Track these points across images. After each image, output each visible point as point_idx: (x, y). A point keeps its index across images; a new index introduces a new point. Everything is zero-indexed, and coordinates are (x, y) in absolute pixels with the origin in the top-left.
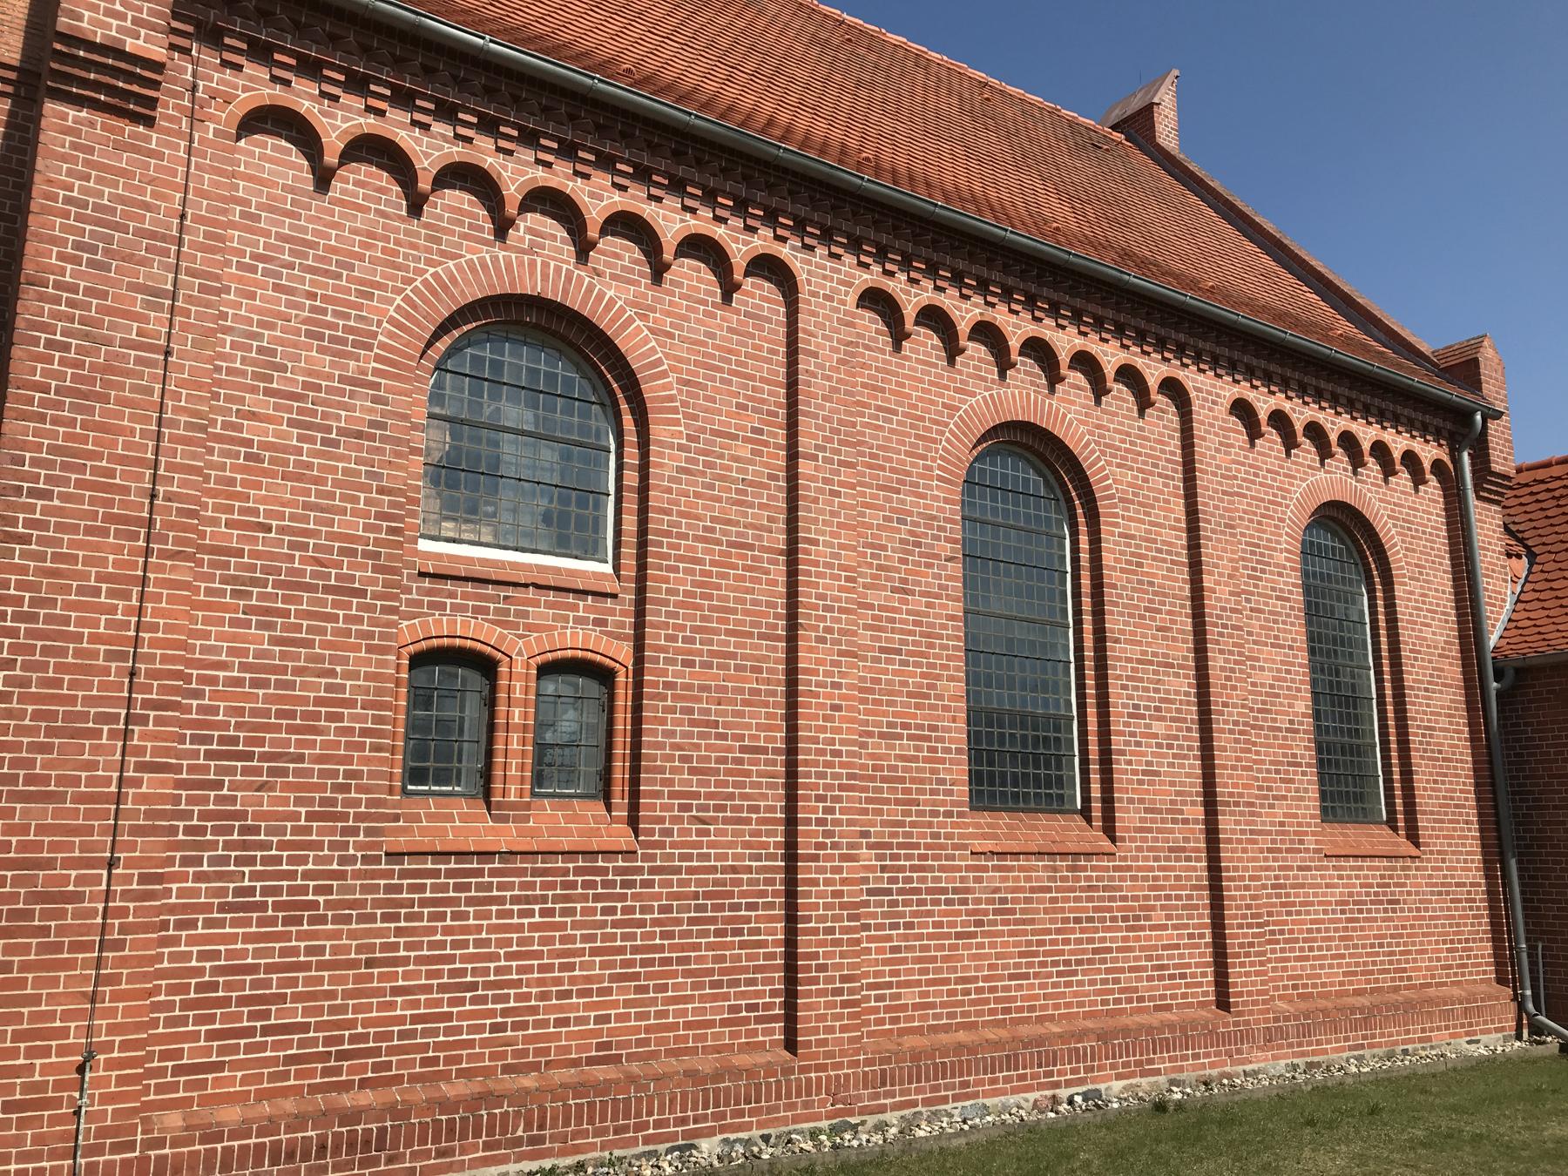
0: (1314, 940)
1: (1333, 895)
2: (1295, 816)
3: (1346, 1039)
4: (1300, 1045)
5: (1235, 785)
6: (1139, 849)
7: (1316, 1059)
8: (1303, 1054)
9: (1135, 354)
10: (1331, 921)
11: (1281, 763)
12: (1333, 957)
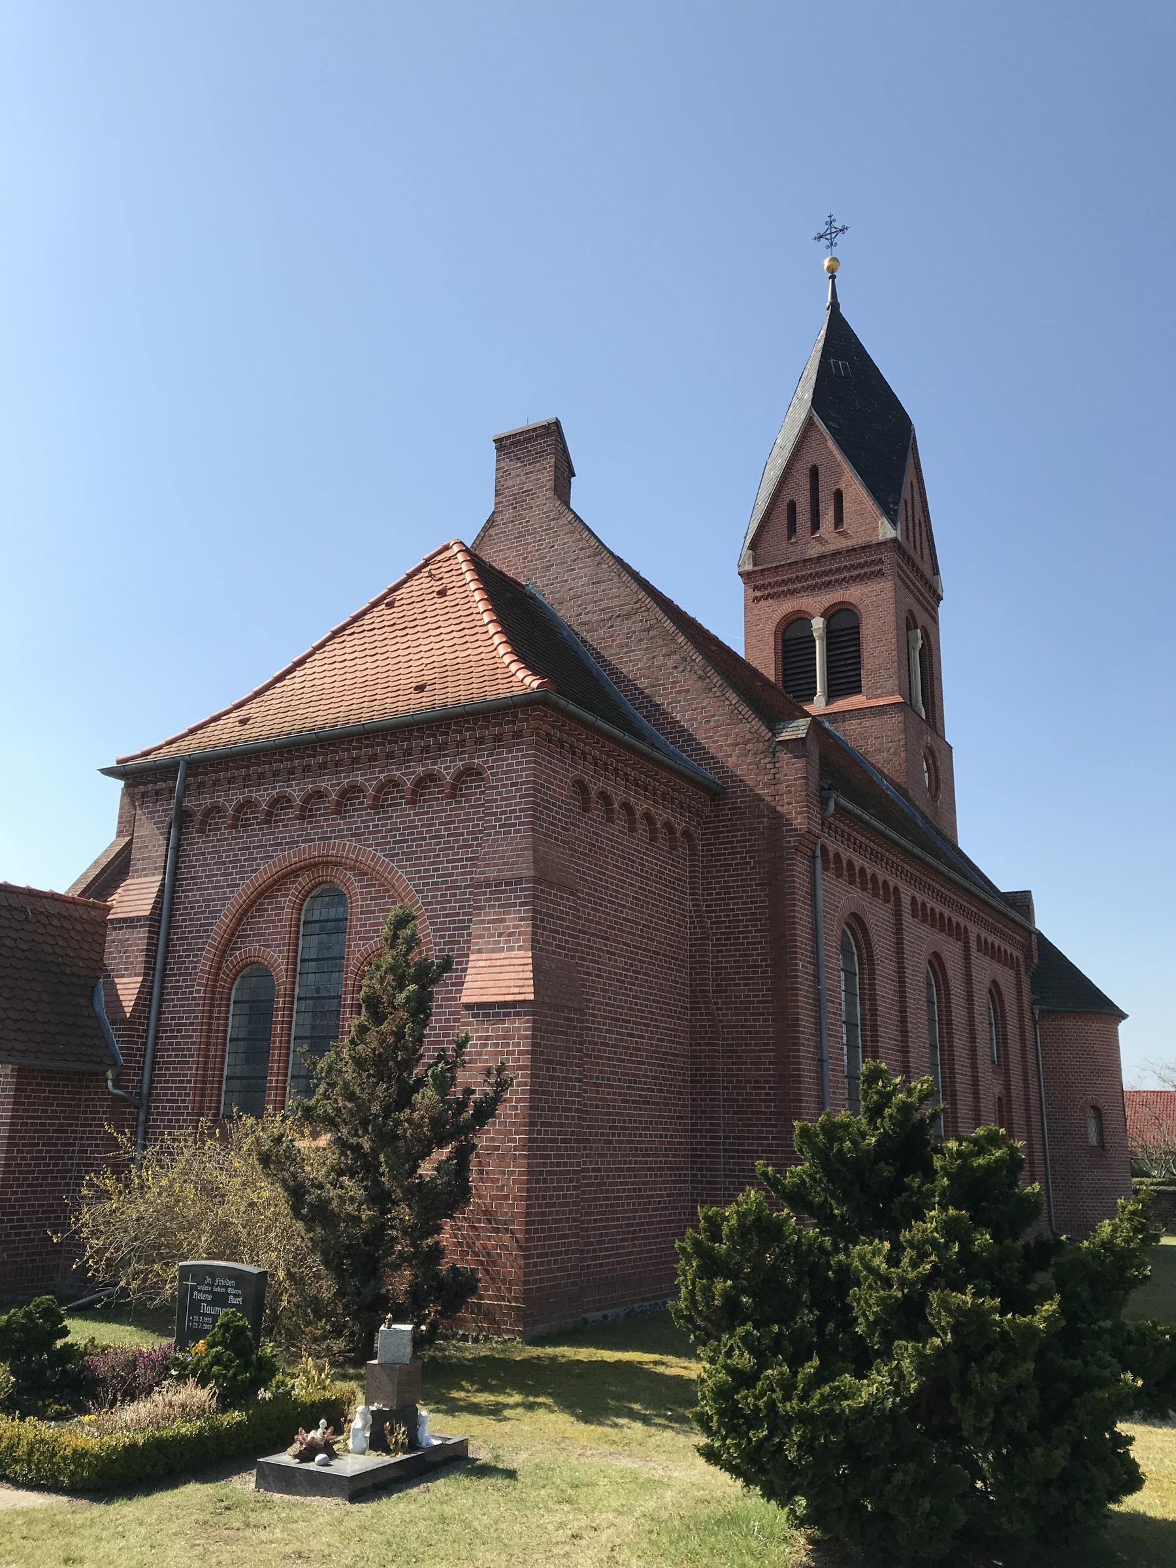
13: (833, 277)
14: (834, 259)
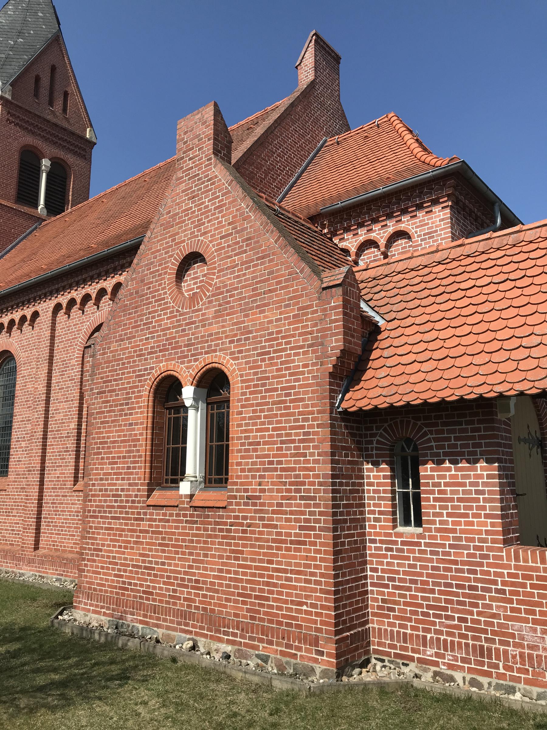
0: (64, 527)
1: (74, 508)
2: (64, 473)
3: (57, 570)
4: (39, 568)
5: (34, 463)
6: (13, 488)
7: (43, 575)
8: (39, 572)
9: (87, 288)
10: (72, 520)
11: (61, 452)
12: (71, 535)
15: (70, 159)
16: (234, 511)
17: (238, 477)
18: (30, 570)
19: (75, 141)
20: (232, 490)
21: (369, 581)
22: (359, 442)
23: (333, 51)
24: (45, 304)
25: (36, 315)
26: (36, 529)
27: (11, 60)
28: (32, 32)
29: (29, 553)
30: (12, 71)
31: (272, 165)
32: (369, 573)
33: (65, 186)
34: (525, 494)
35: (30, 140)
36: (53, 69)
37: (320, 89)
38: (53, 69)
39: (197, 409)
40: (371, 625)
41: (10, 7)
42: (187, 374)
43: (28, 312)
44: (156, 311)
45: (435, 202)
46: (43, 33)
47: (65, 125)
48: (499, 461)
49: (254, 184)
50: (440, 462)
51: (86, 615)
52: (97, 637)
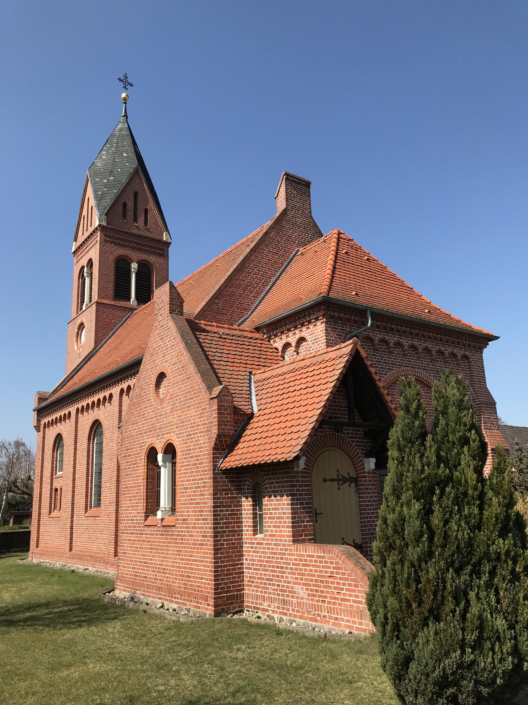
13: (126, 103)
14: (127, 95)
15: (152, 259)
16: (177, 528)
17: (180, 508)
18: (113, 570)
19: (155, 244)
20: (177, 516)
21: (244, 566)
22: (237, 485)
23: (302, 181)
24: (116, 388)
25: (111, 395)
26: (115, 543)
27: (105, 195)
28: (119, 170)
29: (112, 559)
30: (106, 204)
31: (249, 282)
32: (244, 562)
33: (150, 280)
34: (322, 513)
35: (121, 251)
36: (136, 194)
37: (291, 213)
38: (136, 194)
39: (165, 467)
40: (245, 592)
41: (104, 153)
42: (160, 447)
43: (107, 394)
44: (147, 407)
45: (317, 319)
46: (127, 169)
47: (147, 234)
48: (291, 495)
49: (234, 299)
50: (270, 496)
51: (121, 593)
52: (117, 602)
